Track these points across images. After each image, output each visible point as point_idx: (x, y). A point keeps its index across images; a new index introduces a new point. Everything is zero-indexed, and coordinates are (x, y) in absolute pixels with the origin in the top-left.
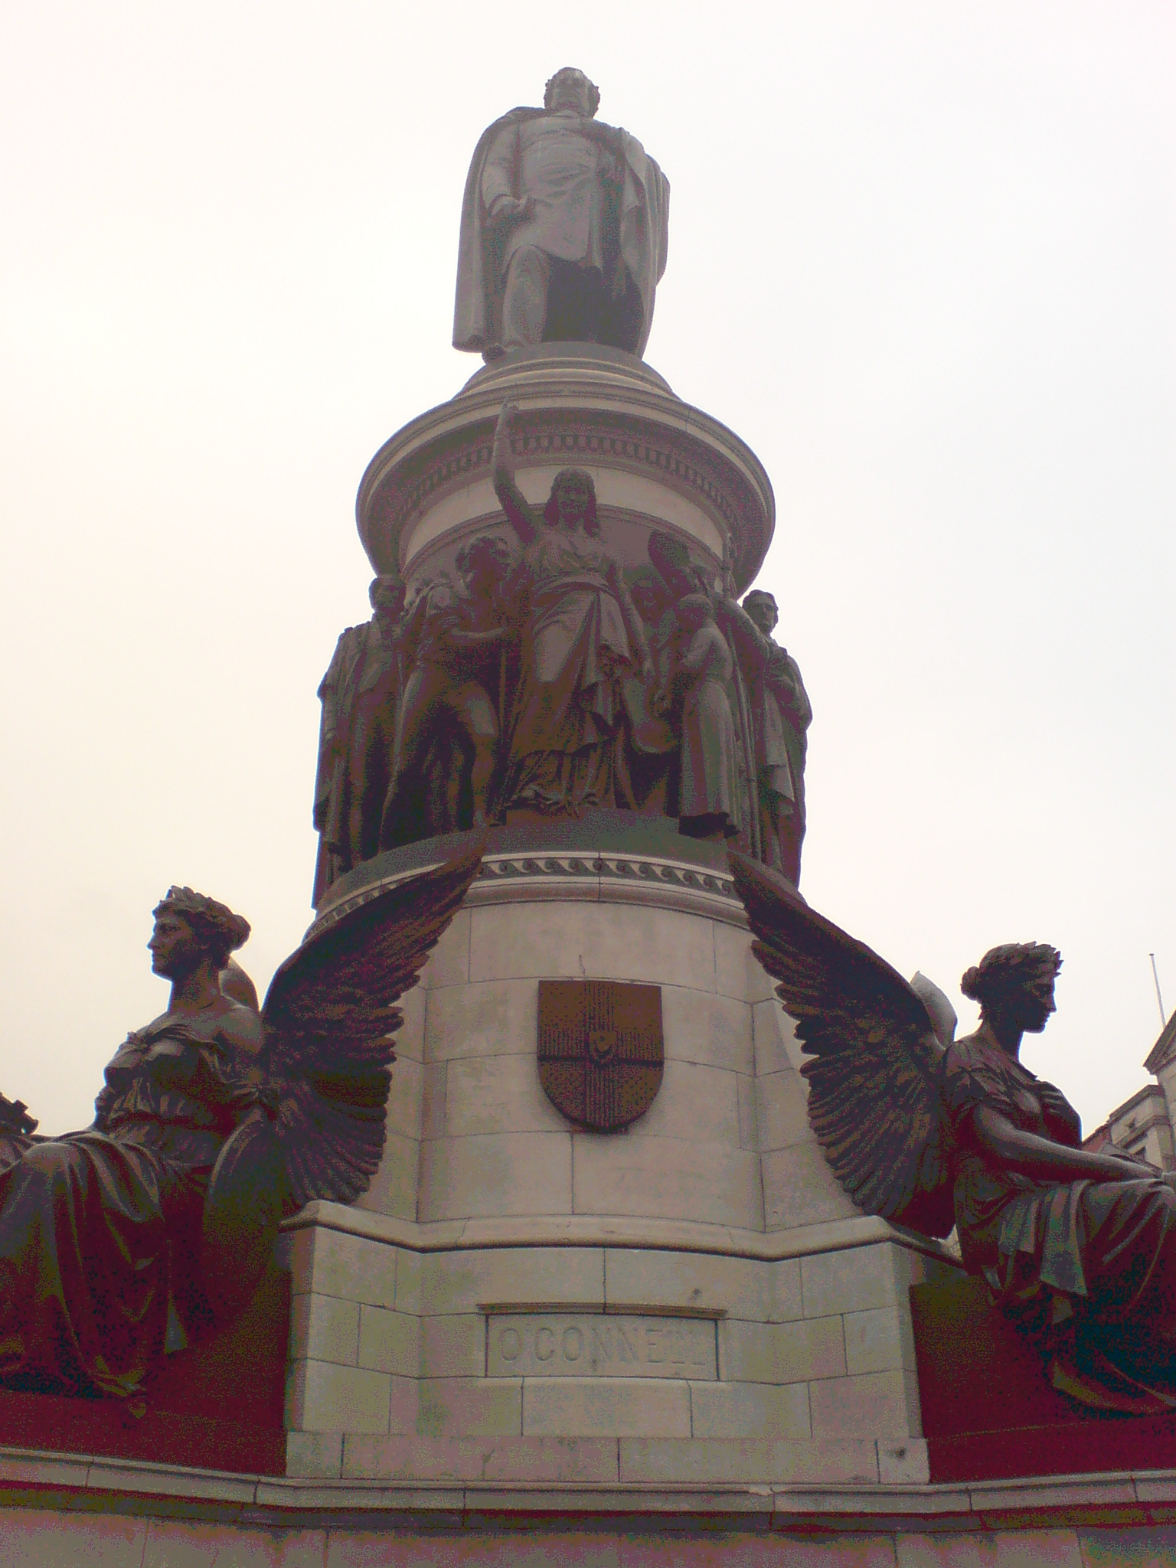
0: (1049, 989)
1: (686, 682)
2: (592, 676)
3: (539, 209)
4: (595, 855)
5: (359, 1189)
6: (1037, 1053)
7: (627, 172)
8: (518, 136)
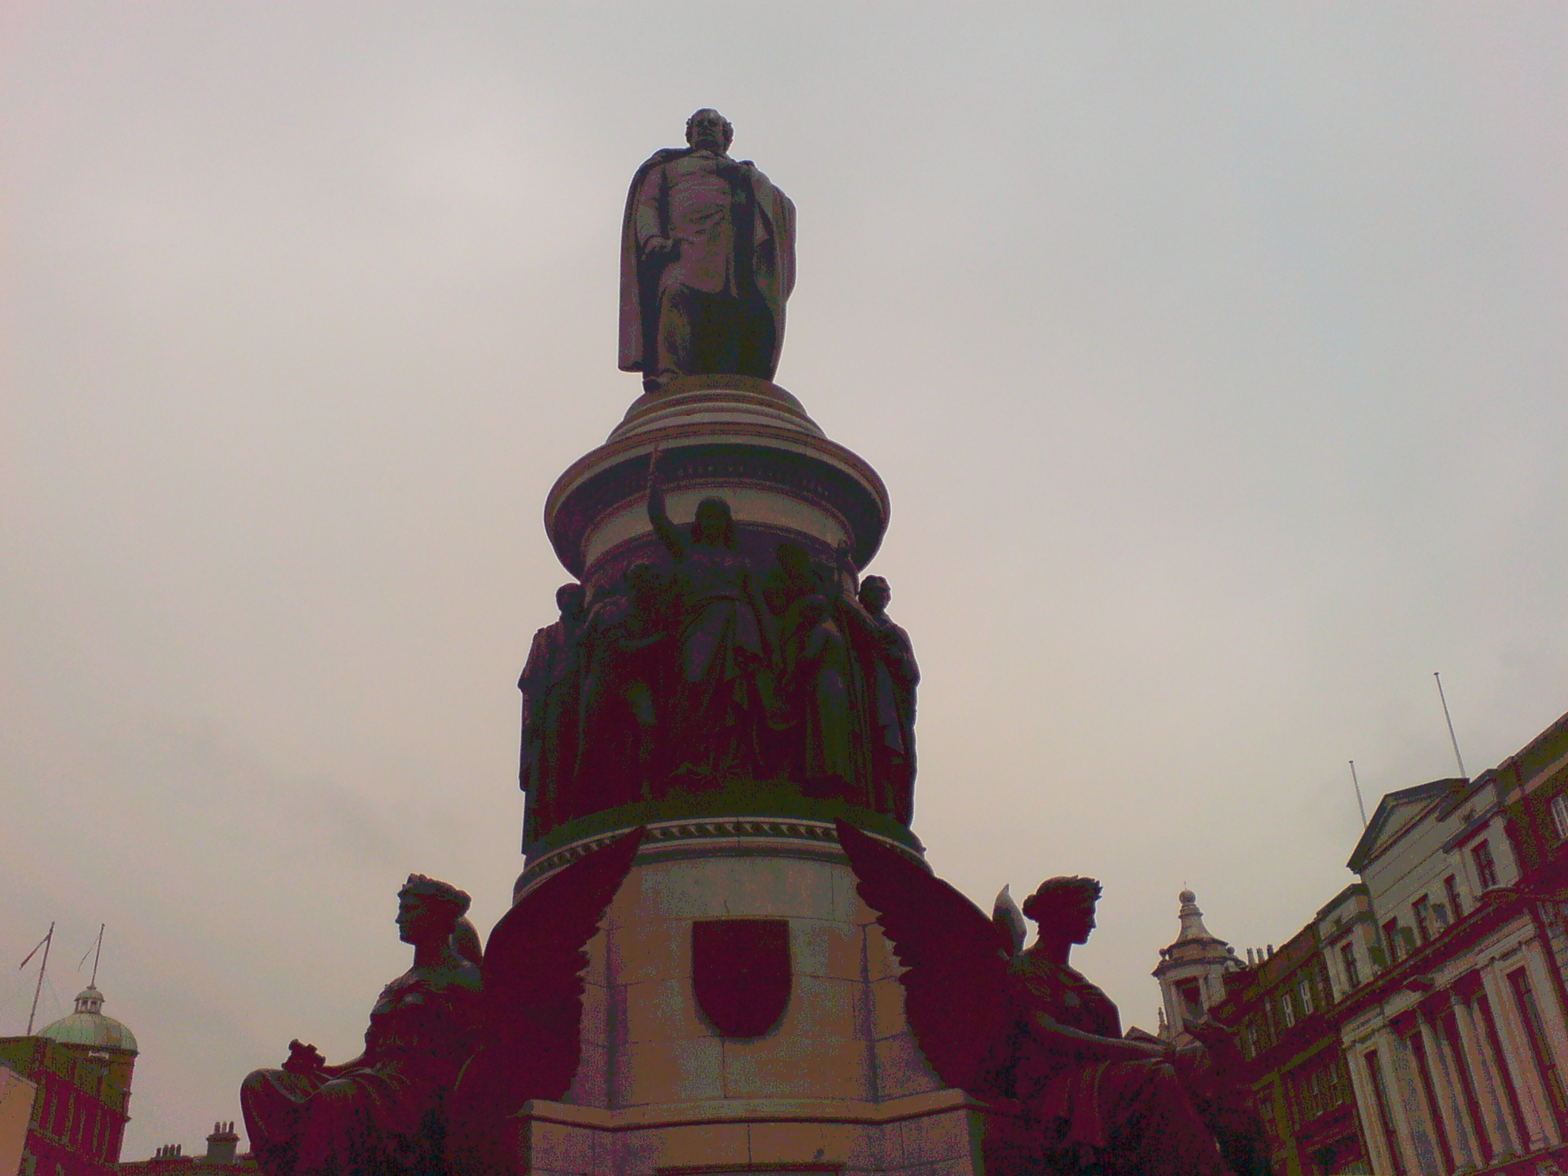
0: (1091, 911)
1: (807, 669)
2: (731, 672)
3: (685, 246)
4: (734, 819)
5: (567, 1086)
6: (1080, 958)
7: (758, 216)
8: (664, 177)
